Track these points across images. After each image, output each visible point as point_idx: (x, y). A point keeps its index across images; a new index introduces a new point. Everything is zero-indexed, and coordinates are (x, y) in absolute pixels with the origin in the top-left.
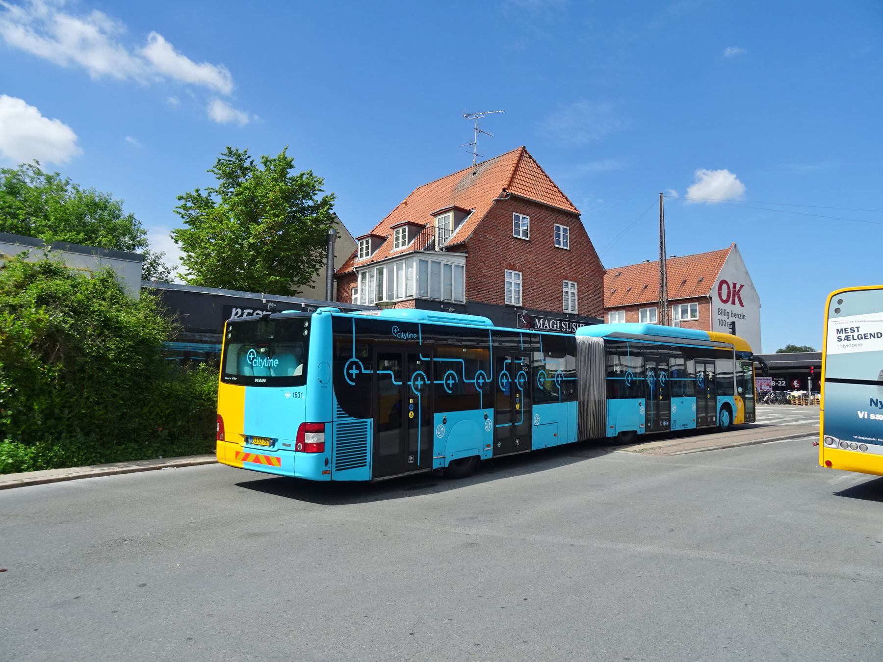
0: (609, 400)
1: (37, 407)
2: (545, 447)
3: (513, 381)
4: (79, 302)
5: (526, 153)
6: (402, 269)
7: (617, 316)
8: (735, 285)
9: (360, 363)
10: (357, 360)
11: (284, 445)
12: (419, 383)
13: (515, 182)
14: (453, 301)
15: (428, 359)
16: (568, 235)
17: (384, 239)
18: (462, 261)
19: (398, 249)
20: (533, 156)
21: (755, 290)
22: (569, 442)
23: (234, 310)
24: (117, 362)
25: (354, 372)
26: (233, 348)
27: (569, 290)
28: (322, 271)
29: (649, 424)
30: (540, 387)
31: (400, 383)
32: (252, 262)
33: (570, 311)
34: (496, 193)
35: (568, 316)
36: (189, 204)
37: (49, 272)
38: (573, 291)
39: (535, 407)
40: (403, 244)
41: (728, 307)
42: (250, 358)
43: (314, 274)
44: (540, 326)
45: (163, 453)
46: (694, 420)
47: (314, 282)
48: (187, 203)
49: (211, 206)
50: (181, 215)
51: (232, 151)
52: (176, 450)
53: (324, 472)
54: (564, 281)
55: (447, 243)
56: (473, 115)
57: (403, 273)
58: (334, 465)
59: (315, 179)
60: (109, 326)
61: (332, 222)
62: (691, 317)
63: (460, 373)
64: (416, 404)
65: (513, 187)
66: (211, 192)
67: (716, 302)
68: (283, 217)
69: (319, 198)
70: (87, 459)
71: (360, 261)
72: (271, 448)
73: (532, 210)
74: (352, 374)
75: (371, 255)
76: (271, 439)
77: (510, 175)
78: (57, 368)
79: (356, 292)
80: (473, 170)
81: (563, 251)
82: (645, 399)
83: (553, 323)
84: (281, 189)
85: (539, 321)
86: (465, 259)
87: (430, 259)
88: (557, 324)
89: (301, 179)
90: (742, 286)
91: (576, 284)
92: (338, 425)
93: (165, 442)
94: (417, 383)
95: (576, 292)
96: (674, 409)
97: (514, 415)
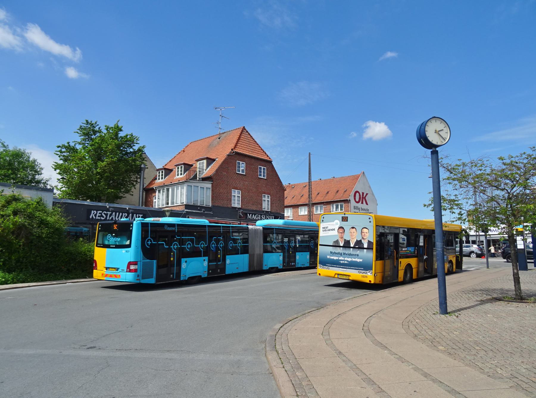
0: (265, 254)
1: (13, 258)
2: (232, 273)
3: (217, 245)
4: (30, 213)
5: (245, 129)
6: (179, 189)
7: (303, 209)
8: (363, 193)
9: (152, 239)
10: (150, 238)
11: (122, 270)
12: (176, 247)
13: (238, 145)
14: (204, 205)
15: (180, 237)
16: (266, 171)
17: (171, 170)
18: (210, 186)
19: (178, 177)
20: (248, 131)
21: (374, 196)
22: (244, 271)
23: (92, 211)
24: (46, 238)
25: (149, 243)
26: (101, 234)
27: (266, 199)
28: (137, 186)
29: (285, 264)
30: (187, 250)
31: (168, 247)
32: (98, 182)
33: (266, 210)
34: (228, 151)
35: (265, 212)
36: (64, 150)
37: (15, 199)
38: (268, 200)
39: (227, 257)
40: (181, 174)
41: (359, 205)
42: (108, 238)
43: (133, 188)
44: (250, 218)
45: (65, 278)
46: (308, 263)
47: (132, 192)
48: (62, 149)
49: (76, 151)
50: (58, 156)
51: (88, 122)
52: (71, 277)
53: (137, 280)
54: (263, 195)
55: (203, 176)
56: (219, 108)
57: (179, 191)
58: (141, 277)
59: (135, 137)
60: (43, 223)
61: (144, 160)
62: (340, 210)
63: (193, 243)
64: (174, 255)
65: (237, 148)
66: (76, 144)
67: (353, 203)
68: (116, 158)
69: (136, 147)
70: (34, 280)
71: (159, 181)
72: (116, 272)
73: (246, 159)
74: (148, 244)
75: (164, 179)
76: (117, 268)
77: (236, 142)
78: (22, 241)
79: (155, 199)
80: (219, 136)
81: (263, 180)
82: (309, 253)
83: (257, 216)
84: (115, 144)
85: (250, 215)
86: (211, 184)
87: (193, 185)
88: (259, 216)
89: (126, 138)
90: (367, 194)
91: (270, 196)
92: (143, 262)
93: (66, 273)
94: (175, 246)
95: (270, 200)
96: (297, 257)
97: (217, 260)
